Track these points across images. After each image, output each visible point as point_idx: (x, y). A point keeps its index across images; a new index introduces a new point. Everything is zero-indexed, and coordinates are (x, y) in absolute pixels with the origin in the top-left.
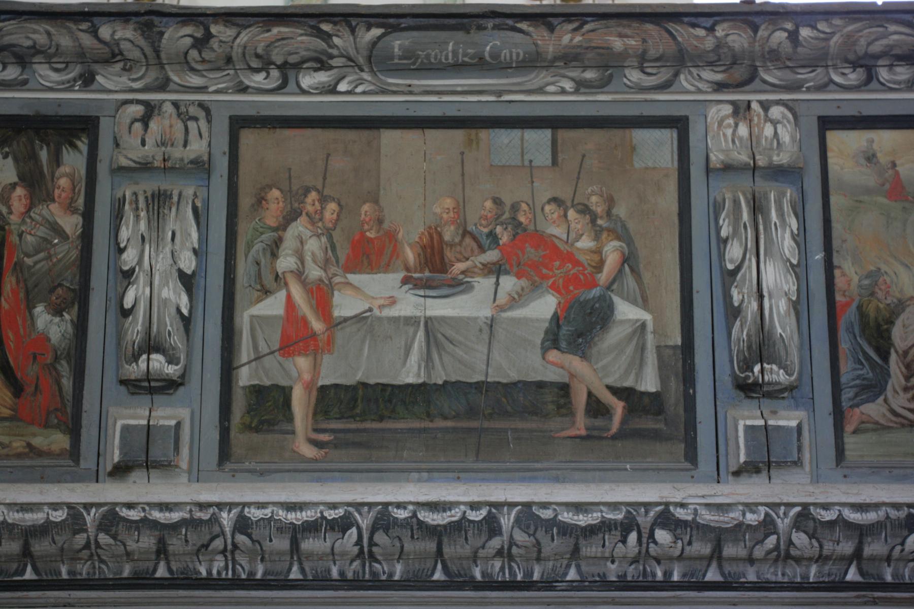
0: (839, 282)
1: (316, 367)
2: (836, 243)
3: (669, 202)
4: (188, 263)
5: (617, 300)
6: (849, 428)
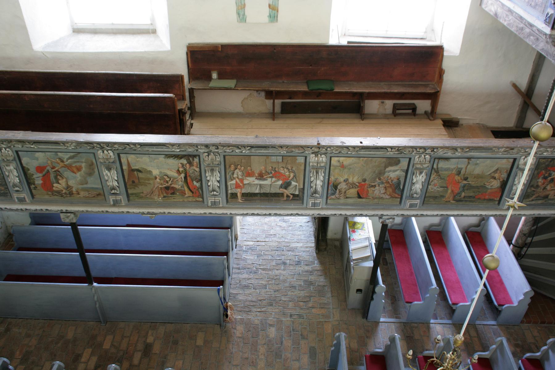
0: (330, 179)
1: (241, 190)
2: (331, 174)
3: (303, 167)
4: (218, 179)
5: (292, 182)
6: (329, 199)
